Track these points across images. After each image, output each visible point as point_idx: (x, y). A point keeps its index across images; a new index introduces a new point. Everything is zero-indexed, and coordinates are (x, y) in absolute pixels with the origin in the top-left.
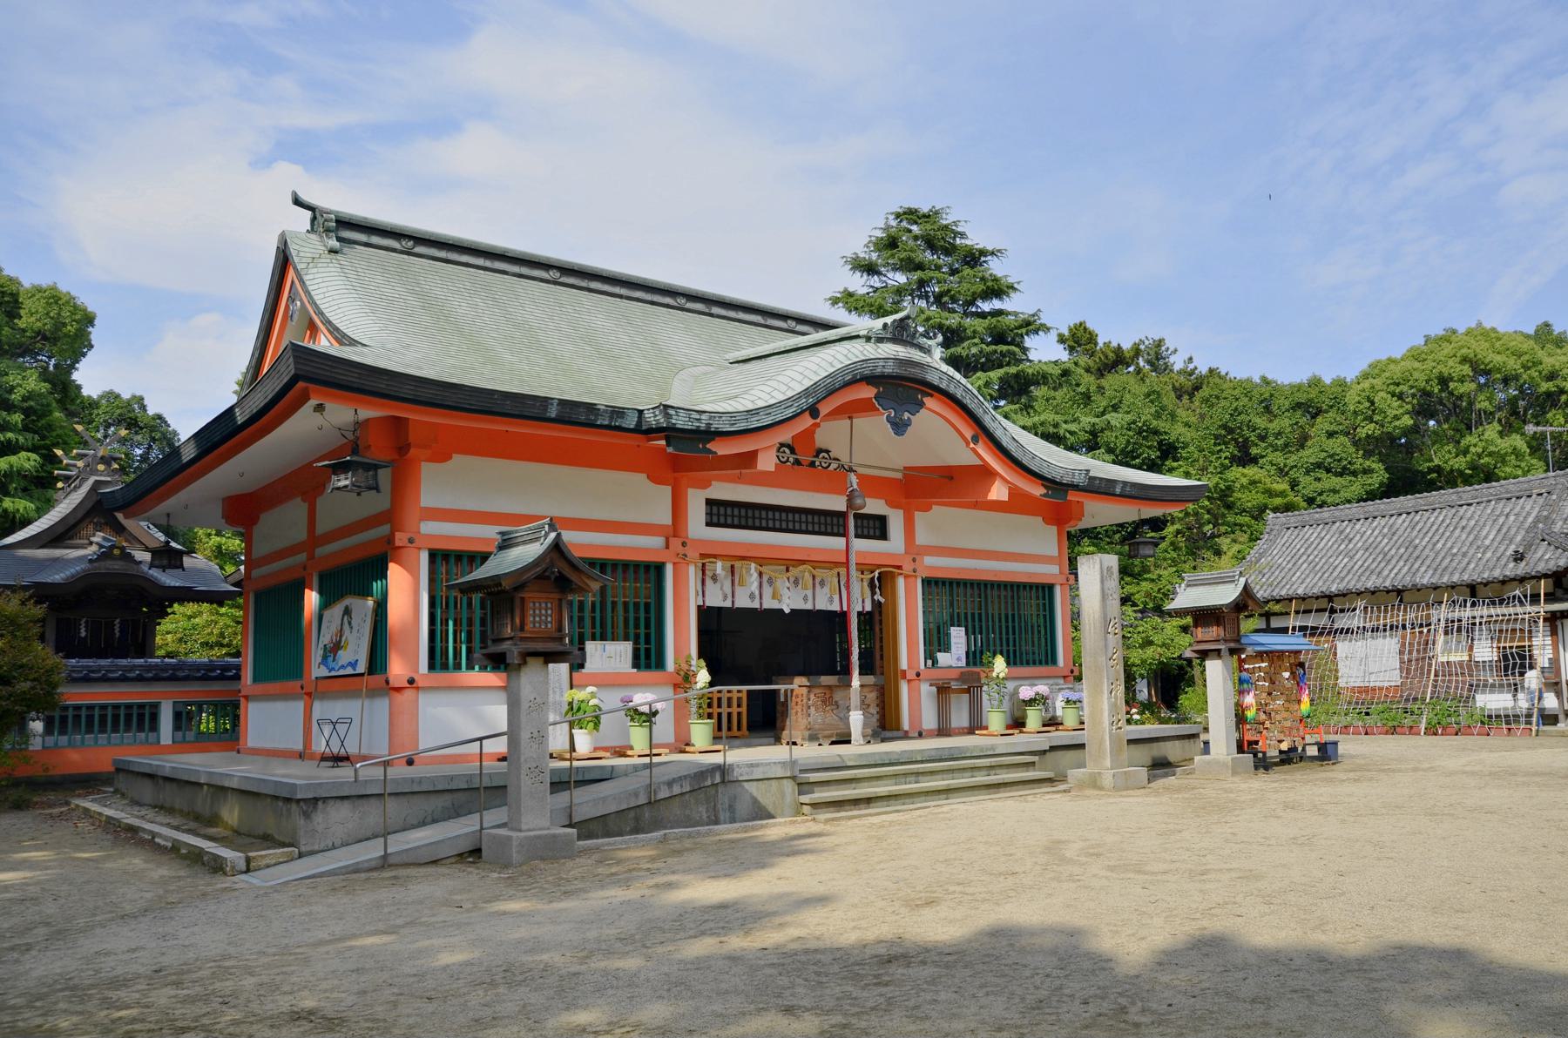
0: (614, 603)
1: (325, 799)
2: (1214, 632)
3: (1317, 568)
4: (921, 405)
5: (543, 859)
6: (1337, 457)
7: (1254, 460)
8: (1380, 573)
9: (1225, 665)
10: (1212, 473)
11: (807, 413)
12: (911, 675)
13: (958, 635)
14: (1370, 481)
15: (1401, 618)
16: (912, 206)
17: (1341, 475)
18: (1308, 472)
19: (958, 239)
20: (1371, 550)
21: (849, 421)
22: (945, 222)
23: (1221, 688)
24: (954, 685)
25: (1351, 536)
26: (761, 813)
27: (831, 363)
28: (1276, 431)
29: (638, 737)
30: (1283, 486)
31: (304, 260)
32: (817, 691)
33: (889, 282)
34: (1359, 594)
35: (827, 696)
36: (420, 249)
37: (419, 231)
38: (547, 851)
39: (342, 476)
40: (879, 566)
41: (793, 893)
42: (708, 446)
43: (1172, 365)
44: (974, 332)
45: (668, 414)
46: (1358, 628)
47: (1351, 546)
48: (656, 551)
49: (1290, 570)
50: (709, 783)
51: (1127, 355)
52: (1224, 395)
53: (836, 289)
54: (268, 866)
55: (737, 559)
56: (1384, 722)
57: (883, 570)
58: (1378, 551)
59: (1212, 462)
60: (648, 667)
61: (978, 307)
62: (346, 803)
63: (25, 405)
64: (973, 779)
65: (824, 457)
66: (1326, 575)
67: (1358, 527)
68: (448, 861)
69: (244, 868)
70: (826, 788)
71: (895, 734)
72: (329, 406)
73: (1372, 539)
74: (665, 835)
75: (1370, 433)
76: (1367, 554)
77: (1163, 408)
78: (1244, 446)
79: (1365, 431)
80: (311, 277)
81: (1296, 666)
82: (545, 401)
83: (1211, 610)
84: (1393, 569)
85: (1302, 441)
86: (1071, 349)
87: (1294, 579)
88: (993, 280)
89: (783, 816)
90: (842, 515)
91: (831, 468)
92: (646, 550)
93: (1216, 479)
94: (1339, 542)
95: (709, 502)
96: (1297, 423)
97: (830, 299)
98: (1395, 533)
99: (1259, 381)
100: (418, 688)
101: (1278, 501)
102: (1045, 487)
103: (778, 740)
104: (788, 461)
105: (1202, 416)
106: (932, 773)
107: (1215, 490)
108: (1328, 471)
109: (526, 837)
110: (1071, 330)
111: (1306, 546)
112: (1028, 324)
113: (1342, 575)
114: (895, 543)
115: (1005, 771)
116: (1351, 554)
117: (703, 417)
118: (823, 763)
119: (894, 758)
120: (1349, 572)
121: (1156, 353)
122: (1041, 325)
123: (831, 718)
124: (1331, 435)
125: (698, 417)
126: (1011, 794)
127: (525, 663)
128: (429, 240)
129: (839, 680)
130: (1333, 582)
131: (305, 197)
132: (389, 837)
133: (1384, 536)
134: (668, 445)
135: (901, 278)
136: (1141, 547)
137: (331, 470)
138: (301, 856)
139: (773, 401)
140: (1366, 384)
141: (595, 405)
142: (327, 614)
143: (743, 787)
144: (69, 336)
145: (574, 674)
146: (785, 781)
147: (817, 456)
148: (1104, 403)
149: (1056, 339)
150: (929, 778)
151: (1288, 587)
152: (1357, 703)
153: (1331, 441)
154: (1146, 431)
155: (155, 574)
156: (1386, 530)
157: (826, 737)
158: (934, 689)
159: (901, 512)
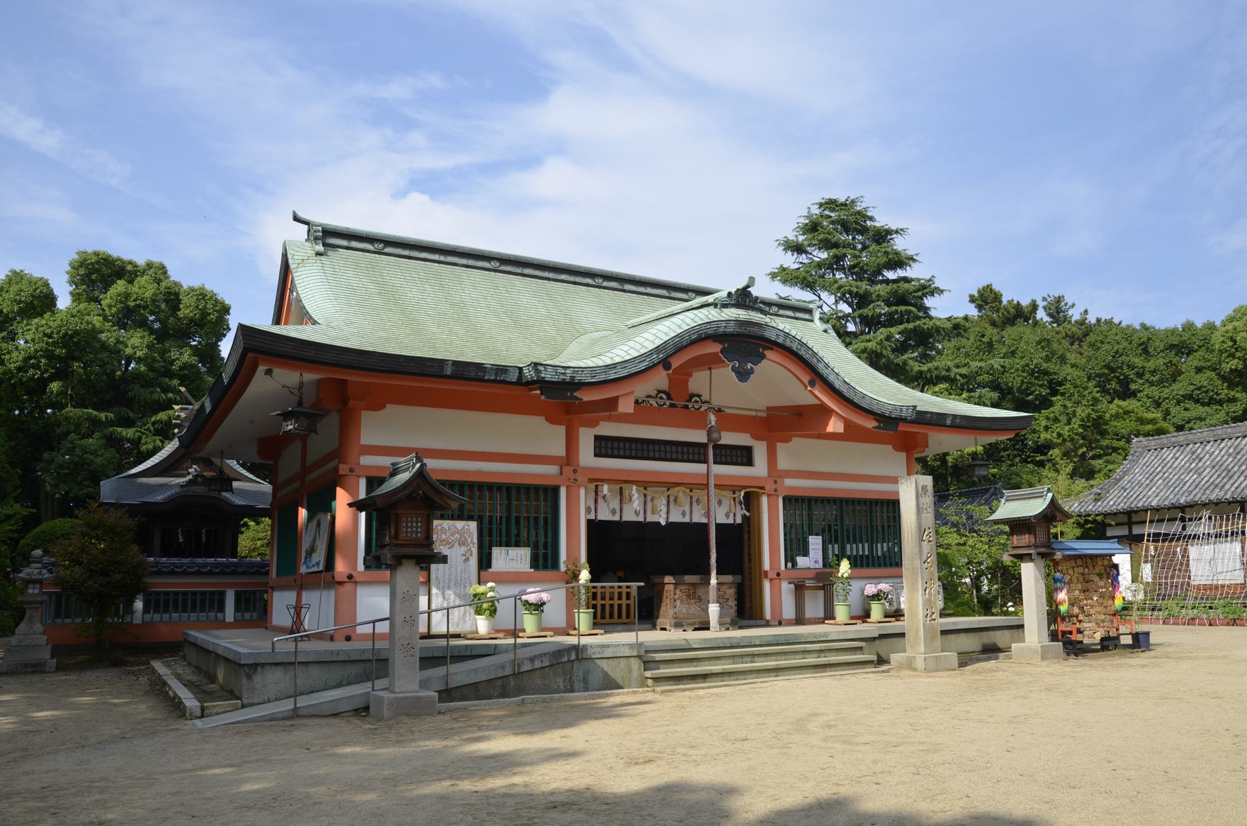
0: (518, 518)
1: (263, 665)
2: (1026, 539)
3: (1170, 484)
4: (763, 357)
5: (409, 715)
6: (1204, 389)
7: (1133, 394)
8: (1223, 487)
9: (1037, 566)
10: (1085, 406)
11: (661, 366)
12: (772, 575)
13: (815, 542)
14: (1234, 409)
15: (1240, 526)
16: (832, 198)
17: (1208, 404)
18: (1178, 403)
19: (868, 222)
20: (1217, 468)
21: (708, 371)
22: (858, 208)
23: (1033, 586)
24: (808, 583)
25: (1201, 456)
26: (611, 684)
27: (679, 326)
28: (1152, 369)
29: (529, 623)
30: (1158, 415)
31: (297, 261)
32: (683, 587)
33: (815, 258)
34: (1205, 505)
35: (691, 592)
36: (388, 250)
37: (388, 236)
38: (413, 709)
39: (289, 423)
40: (745, 487)
41: (557, 749)
42: (575, 394)
43: (1071, 317)
44: (878, 296)
45: (538, 370)
46: (1204, 534)
47: (1200, 464)
48: (552, 476)
49: (1148, 485)
50: (566, 659)
51: (1026, 310)
52: (1107, 340)
53: (774, 266)
54: (218, 714)
55: (622, 483)
56: (1225, 615)
57: (748, 490)
58: (1223, 468)
59: (1085, 396)
60: (545, 567)
61: (883, 276)
62: (279, 668)
63: (182, 373)
64: (820, 659)
65: (696, 402)
66: (1177, 489)
67: (1207, 448)
68: (346, 714)
69: (199, 715)
70: (670, 665)
71: (759, 622)
72: (276, 371)
73: (1219, 458)
74: (523, 699)
75: (1233, 367)
76: (1214, 471)
77: (1053, 353)
78: (1125, 382)
79: (1229, 366)
80: (298, 274)
81: (1111, 567)
82: (442, 362)
83: (1022, 521)
84: (1234, 483)
85: (1175, 376)
86: (980, 307)
87: (1149, 493)
88: (894, 254)
89: (629, 686)
90: (704, 446)
91: (702, 409)
92: (544, 476)
93: (1088, 411)
94: (1191, 461)
95: (598, 438)
96: (1171, 361)
97: (770, 274)
98: (1239, 453)
99: (1138, 327)
100: (356, 583)
101: (1149, 427)
102: (877, 421)
103: (654, 627)
104: (664, 404)
105: (1089, 359)
106: (766, 655)
107: (1088, 419)
108: (1197, 401)
109: (395, 698)
110: (979, 291)
111: (1163, 465)
112: (924, 287)
113: (1190, 489)
114: (760, 468)
115: (834, 654)
116: (1199, 471)
117: (567, 372)
118: (670, 646)
119: (734, 642)
120: (1197, 486)
121: (1056, 307)
122: (935, 288)
123: (694, 609)
124: (1199, 370)
125: (564, 371)
126: (788, 677)
127: (400, 564)
128: (396, 243)
129: (701, 579)
130: (1182, 495)
131: (302, 215)
132: (298, 698)
133: (1229, 456)
134: (542, 394)
135: (824, 255)
136: (977, 468)
137: (282, 418)
138: (243, 706)
139: (628, 358)
140: (1230, 327)
141: (483, 364)
142: (310, 525)
143: (596, 664)
144: (212, 323)
145: (482, 573)
146: (632, 660)
147: (689, 401)
148: (1004, 350)
149: (968, 299)
150: (763, 659)
151: (1144, 500)
152: (1202, 599)
153: (1198, 377)
154: (1037, 372)
155: (228, 496)
156: (1231, 450)
157: (689, 624)
158: (792, 586)
159: (765, 443)
